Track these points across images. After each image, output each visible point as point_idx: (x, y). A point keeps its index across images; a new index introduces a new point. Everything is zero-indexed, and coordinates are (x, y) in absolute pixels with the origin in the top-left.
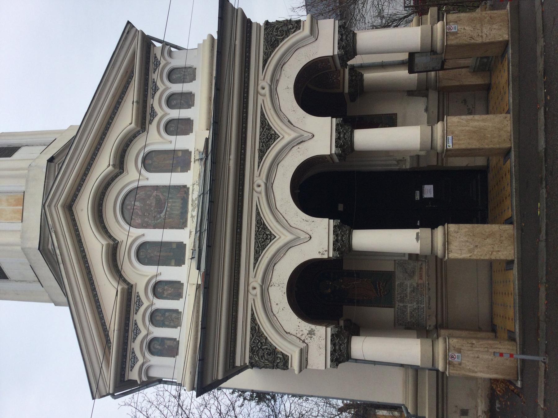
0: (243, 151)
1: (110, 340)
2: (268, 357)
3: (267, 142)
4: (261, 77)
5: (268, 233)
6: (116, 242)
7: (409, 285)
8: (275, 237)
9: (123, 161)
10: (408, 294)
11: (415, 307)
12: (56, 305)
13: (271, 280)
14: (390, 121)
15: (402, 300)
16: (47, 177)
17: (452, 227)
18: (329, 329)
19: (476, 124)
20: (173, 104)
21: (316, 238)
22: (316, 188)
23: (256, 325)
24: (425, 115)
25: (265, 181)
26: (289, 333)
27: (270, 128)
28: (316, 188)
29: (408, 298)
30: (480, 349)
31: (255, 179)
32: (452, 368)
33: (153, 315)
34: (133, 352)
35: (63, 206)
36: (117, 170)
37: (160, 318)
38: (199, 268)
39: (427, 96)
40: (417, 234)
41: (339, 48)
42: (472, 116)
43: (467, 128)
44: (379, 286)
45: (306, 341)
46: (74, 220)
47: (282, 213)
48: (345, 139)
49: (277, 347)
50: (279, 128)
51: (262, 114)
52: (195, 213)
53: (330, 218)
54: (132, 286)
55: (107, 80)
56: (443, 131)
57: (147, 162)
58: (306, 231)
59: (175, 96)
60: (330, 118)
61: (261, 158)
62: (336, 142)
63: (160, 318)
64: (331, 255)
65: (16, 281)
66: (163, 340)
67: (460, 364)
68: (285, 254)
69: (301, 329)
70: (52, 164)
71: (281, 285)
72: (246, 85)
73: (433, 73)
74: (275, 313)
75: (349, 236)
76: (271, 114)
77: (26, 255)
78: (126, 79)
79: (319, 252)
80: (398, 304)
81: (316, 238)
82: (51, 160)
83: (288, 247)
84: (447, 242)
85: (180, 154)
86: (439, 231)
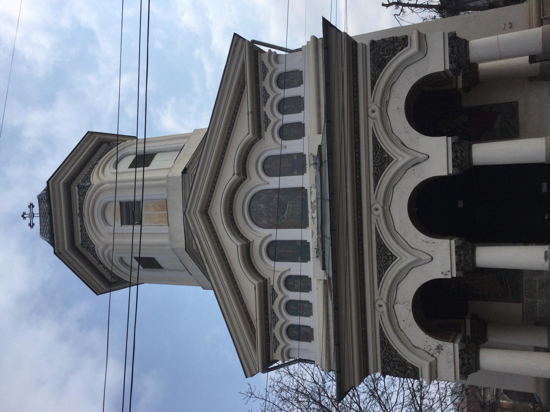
0: (358, 176)
1: (253, 326)
4: (370, 99)
5: (389, 254)
8: (397, 258)
12: (204, 289)
13: (396, 298)
14: (511, 132)
16: (183, 187)
18: (453, 242)
21: (439, 258)
22: (433, 208)
26: (417, 347)
28: (433, 208)
35: (201, 212)
36: (242, 177)
38: (324, 268)
40: (546, 253)
41: (450, 63)
45: (435, 355)
49: (407, 359)
50: (393, 152)
52: (315, 215)
53: (448, 136)
54: (266, 280)
57: (266, 166)
58: (427, 252)
60: (445, 137)
61: (376, 182)
62: (450, 57)
66: (299, 327)
68: (407, 274)
69: (429, 344)
70: (186, 175)
71: (406, 303)
72: (356, 110)
74: (402, 329)
76: (383, 137)
79: (442, 273)
81: (439, 258)
82: (185, 171)
83: (410, 267)
85: (295, 157)
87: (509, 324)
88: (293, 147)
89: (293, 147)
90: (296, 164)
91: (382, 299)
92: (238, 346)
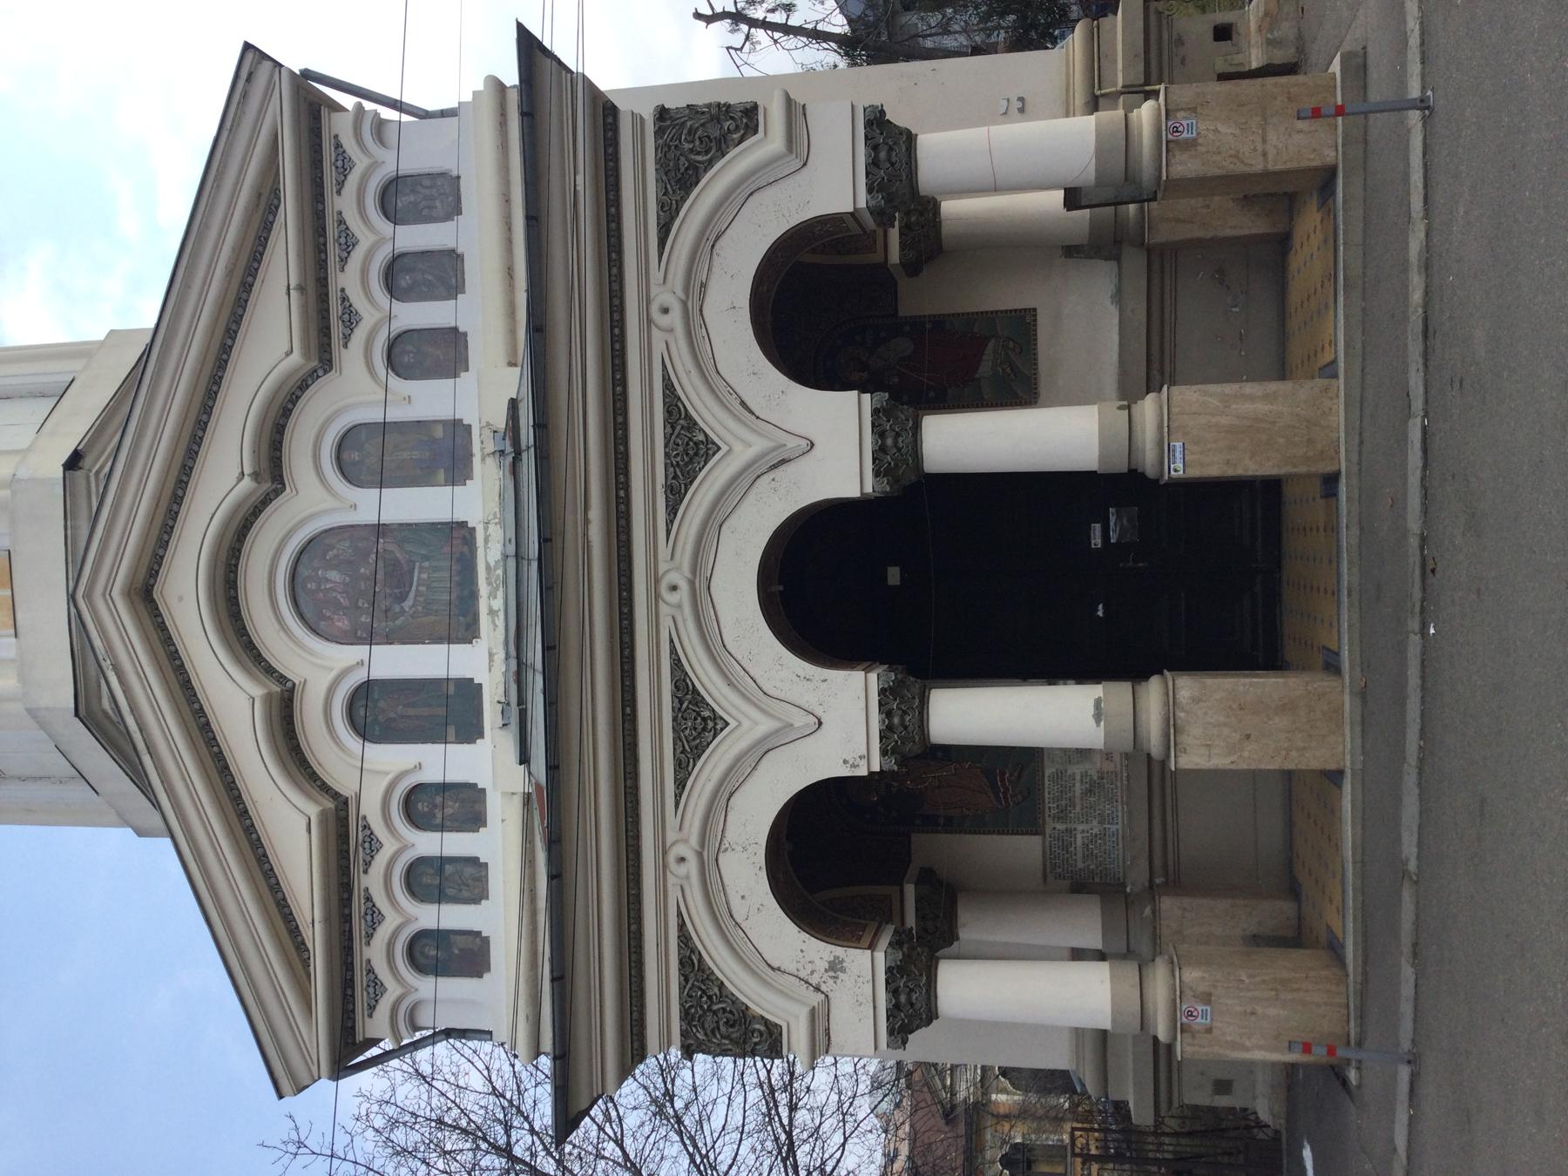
1: (303, 943)
2: (723, 1025)
3: (686, 465)
4: (656, 275)
5: (706, 714)
6: (289, 684)
7: (1078, 777)
8: (727, 724)
9: (280, 458)
10: (1078, 801)
11: (1096, 831)
15: (1062, 816)
17: (1187, 686)
18: (873, 677)
19: (1246, 407)
20: (403, 284)
21: (832, 722)
22: (828, 585)
23: (692, 951)
24: (1113, 311)
25: (689, 576)
27: (692, 425)
28: (828, 585)
29: (1078, 809)
30: (1257, 994)
31: (654, 291)
32: (1188, 1039)
33: (395, 347)
34: (370, 971)
35: (128, 593)
36: (267, 486)
37: (431, 880)
38: (524, 759)
39: (1117, 258)
40: (1098, 702)
41: (870, 190)
42: (1235, 386)
43: (1224, 421)
44: (1003, 780)
45: (823, 988)
46: (162, 627)
47: (739, 658)
48: (893, 164)
51: (668, 386)
52: (498, 604)
54: (346, 802)
55: (205, 226)
56: (1160, 427)
57: (345, 456)
59: (406, 260)
60: (855, 393)
61: (672, 510)
62: (874, 460)
63: (431, 880)
64: (869, 489)
65: (23, 779)
67: (1209, 1030)
73: (1132, 207)
75: (921, 713)
77: (42, 725)
78: (257, 218)
79: (845, 762)
80: (1053, 826)
81: (832, 722)
82: (74, 462)
83: (763, 749)
84: (1172, 726)
85: (439, 432)
86: (1153, 689)
87: (1006, 892)
88: (427, 400)
89: (427, 400)
90: (443, 453)
91: (686, 841)
92: (1154, 63)
